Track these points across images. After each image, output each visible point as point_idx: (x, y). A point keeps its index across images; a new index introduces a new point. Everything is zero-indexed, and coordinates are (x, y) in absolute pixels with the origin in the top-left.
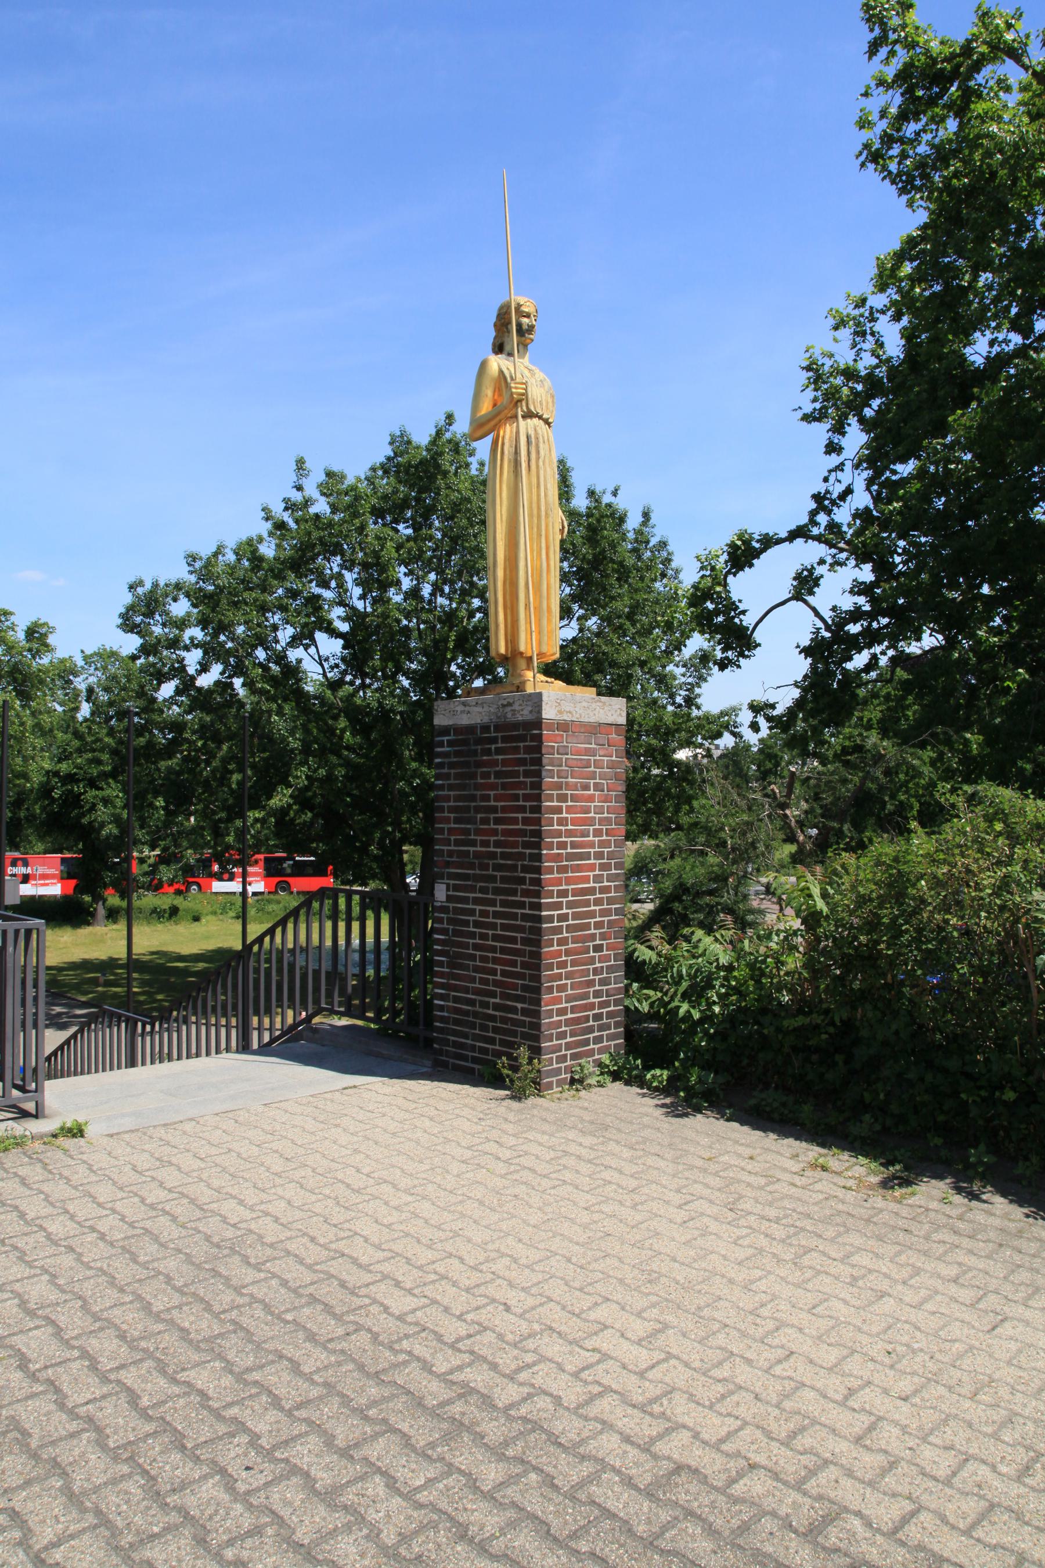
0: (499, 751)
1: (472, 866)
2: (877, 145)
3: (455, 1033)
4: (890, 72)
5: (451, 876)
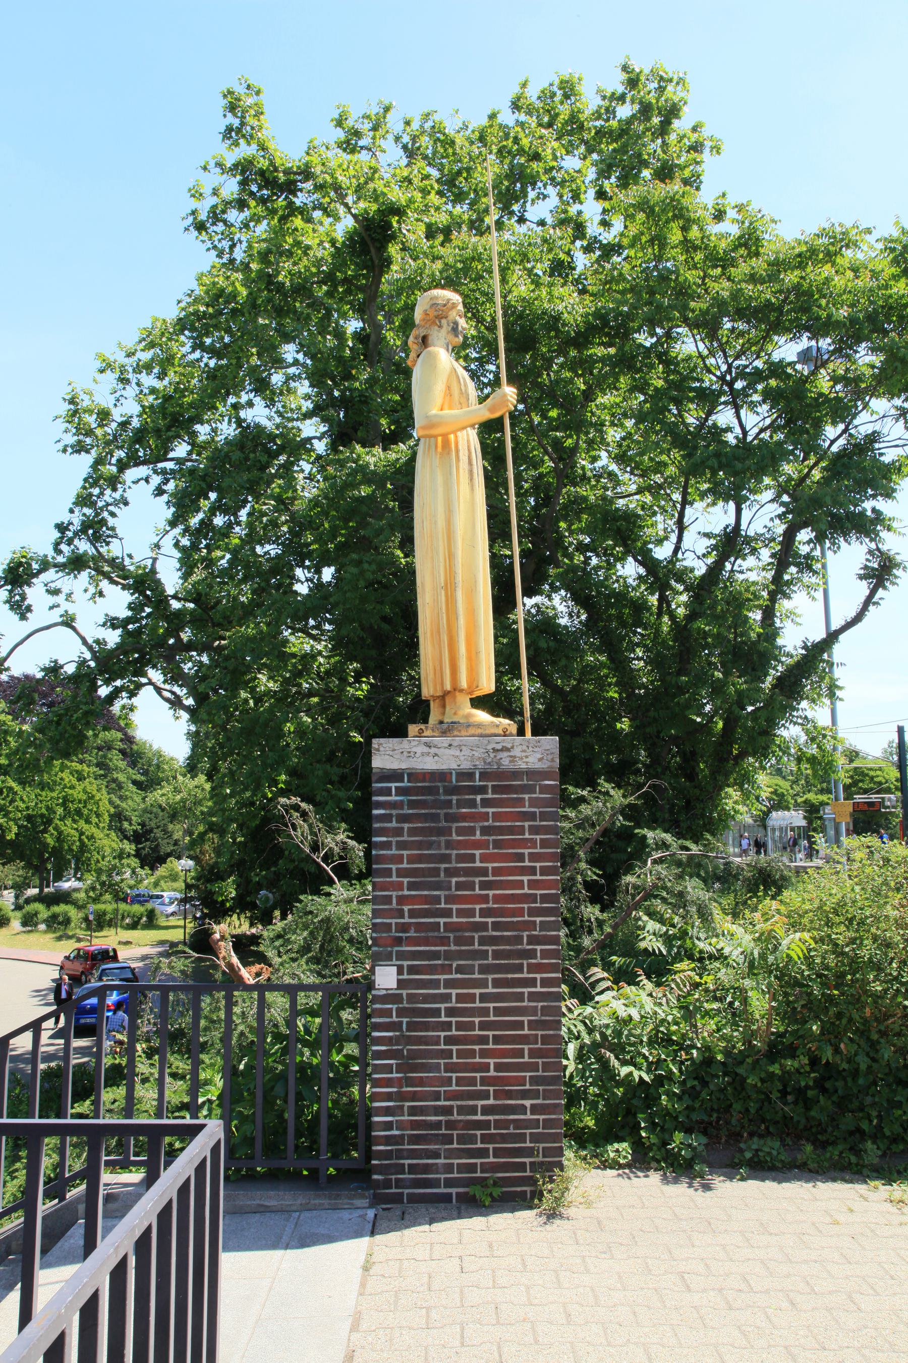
0: (486, 803)
1: (444, 941)
2: (203, 216)
3: (413, 1154)
4: (230, 159)
5: (401, 956)
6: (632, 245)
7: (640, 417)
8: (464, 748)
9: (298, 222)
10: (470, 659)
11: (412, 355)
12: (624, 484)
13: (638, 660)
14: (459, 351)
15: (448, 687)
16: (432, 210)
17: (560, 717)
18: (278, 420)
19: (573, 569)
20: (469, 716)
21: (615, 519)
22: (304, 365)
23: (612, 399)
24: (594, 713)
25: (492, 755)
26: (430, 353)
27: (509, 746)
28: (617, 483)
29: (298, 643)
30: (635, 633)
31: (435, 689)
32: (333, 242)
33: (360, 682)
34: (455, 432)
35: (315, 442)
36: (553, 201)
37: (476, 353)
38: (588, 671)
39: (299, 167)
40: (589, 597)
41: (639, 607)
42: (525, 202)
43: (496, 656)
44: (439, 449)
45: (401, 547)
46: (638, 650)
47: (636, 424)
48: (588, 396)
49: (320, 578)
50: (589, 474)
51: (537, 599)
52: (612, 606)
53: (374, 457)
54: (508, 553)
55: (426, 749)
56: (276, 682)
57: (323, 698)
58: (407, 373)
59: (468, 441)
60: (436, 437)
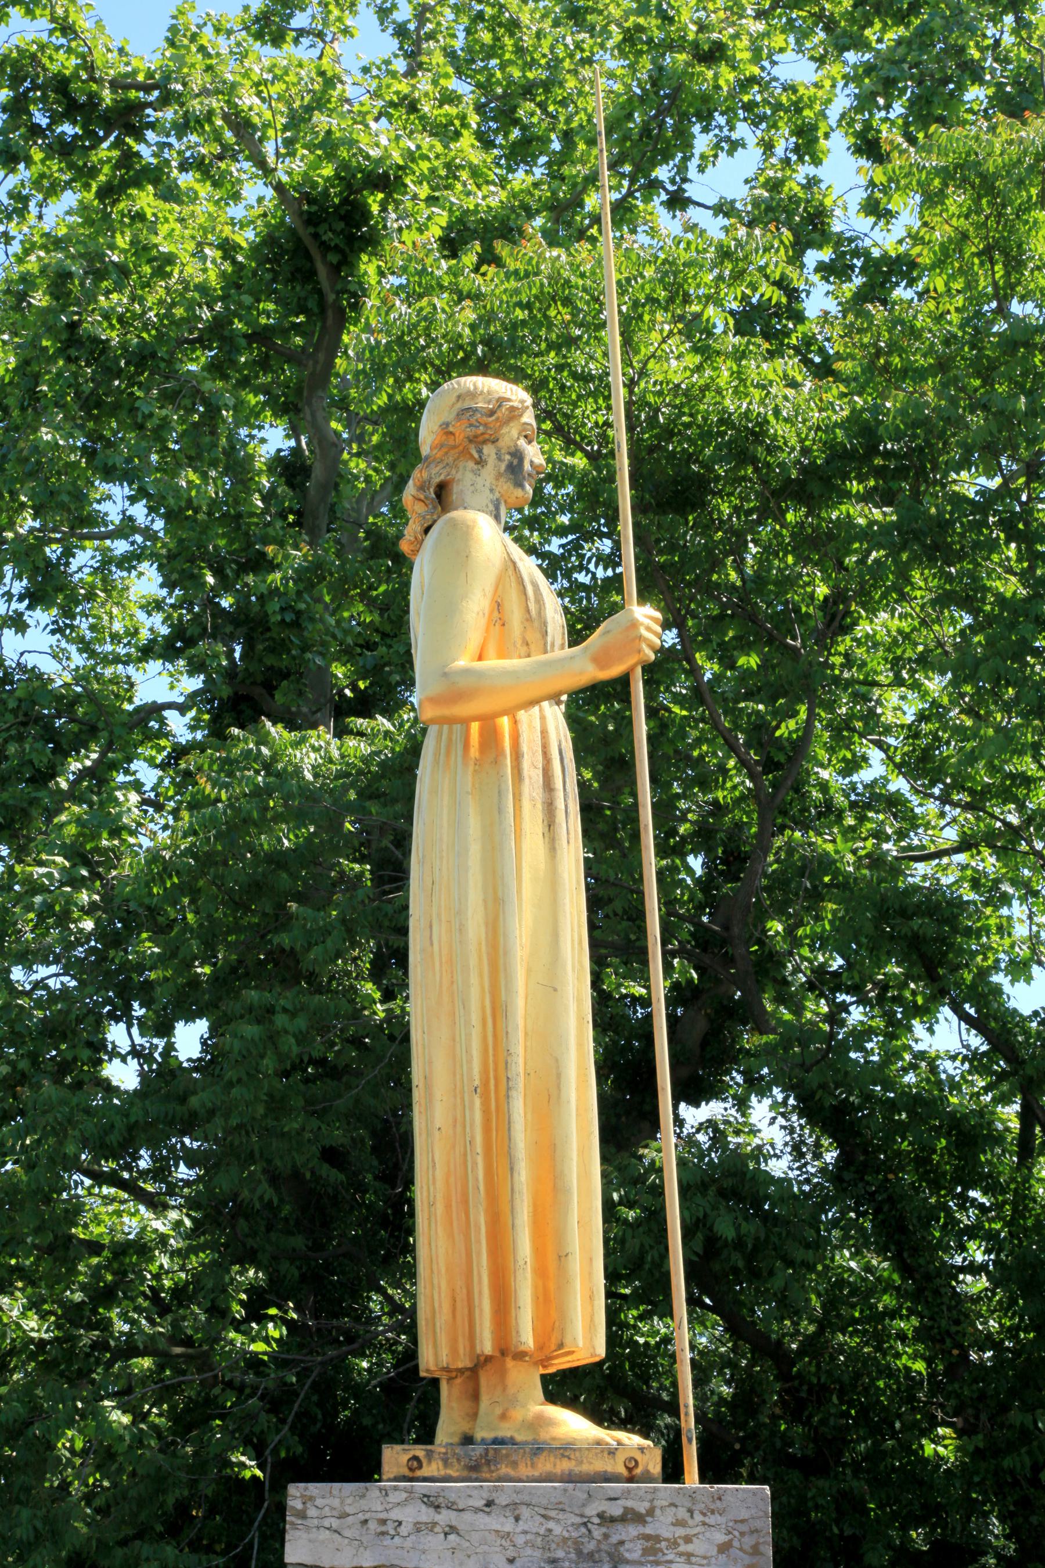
6: (939, 264)
7: (964, 667)
8: (525, 1512)
9: (145, 199)
10: (541, 1272)
11: (412, 529)
12: (927, 826)
13: (973, 1268)
14: (528, 526)
15: (487, 1347)
16: (464, 175)
17: (774, 1418)
18: (78, 660)
19: (805, 1035)
20: (540, 1422)
21: (905, 914)
22: (148, 533)
23: (895, 624)
24: (864, 1411)
25: (597, 1533)
26: (454, 524)
27: (642, 1507)
28: (911, 822)
29: (109, 1215)
30: (964, 1202)
31: (454, 1351)
32: (228, 248)
33: (262, 1319)
34: (511, 712)
35: (172, 717)
36: (749, 159)
37: (560, 518)
38: (841, 1294)
39: (150, 75)
40: (844, 1108)
41: (971, 1134)
42: (686, 159)
43: (608, 1254)
44: (474, 752)
45: (377, 974)
46: (972, 1245)
47: (955, 683)
48: (836, 619)
49: (170, 1047)
50: (840, 800)
51: (713, 1109)
52: (902, 1129)
53: (314, 752)
54: (640, 991)
55: (426, 1514)
56: (43, 1316)
57: (164, 1360)
58: (401, 564)
59: (544, 733)
60: (466, 722)
